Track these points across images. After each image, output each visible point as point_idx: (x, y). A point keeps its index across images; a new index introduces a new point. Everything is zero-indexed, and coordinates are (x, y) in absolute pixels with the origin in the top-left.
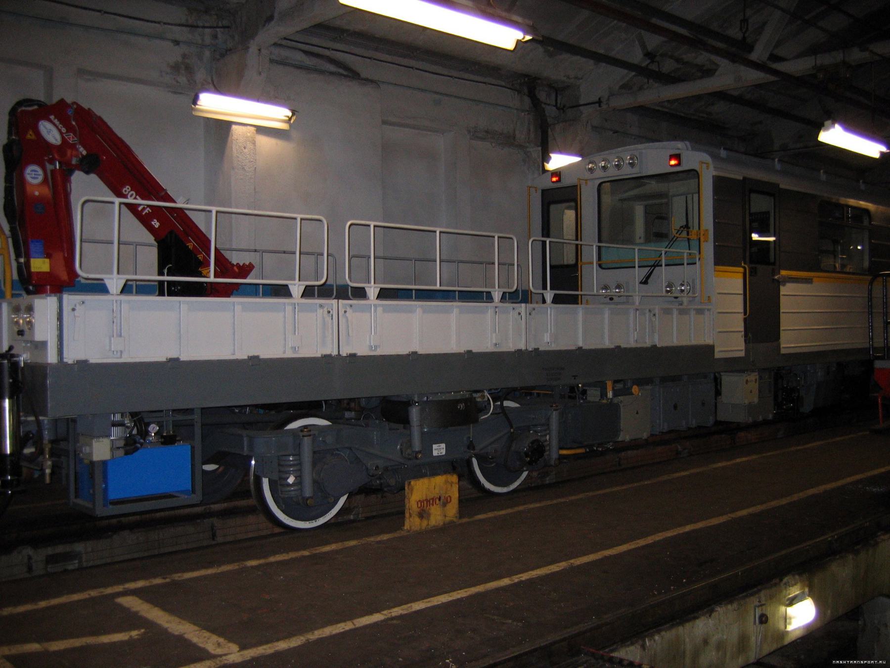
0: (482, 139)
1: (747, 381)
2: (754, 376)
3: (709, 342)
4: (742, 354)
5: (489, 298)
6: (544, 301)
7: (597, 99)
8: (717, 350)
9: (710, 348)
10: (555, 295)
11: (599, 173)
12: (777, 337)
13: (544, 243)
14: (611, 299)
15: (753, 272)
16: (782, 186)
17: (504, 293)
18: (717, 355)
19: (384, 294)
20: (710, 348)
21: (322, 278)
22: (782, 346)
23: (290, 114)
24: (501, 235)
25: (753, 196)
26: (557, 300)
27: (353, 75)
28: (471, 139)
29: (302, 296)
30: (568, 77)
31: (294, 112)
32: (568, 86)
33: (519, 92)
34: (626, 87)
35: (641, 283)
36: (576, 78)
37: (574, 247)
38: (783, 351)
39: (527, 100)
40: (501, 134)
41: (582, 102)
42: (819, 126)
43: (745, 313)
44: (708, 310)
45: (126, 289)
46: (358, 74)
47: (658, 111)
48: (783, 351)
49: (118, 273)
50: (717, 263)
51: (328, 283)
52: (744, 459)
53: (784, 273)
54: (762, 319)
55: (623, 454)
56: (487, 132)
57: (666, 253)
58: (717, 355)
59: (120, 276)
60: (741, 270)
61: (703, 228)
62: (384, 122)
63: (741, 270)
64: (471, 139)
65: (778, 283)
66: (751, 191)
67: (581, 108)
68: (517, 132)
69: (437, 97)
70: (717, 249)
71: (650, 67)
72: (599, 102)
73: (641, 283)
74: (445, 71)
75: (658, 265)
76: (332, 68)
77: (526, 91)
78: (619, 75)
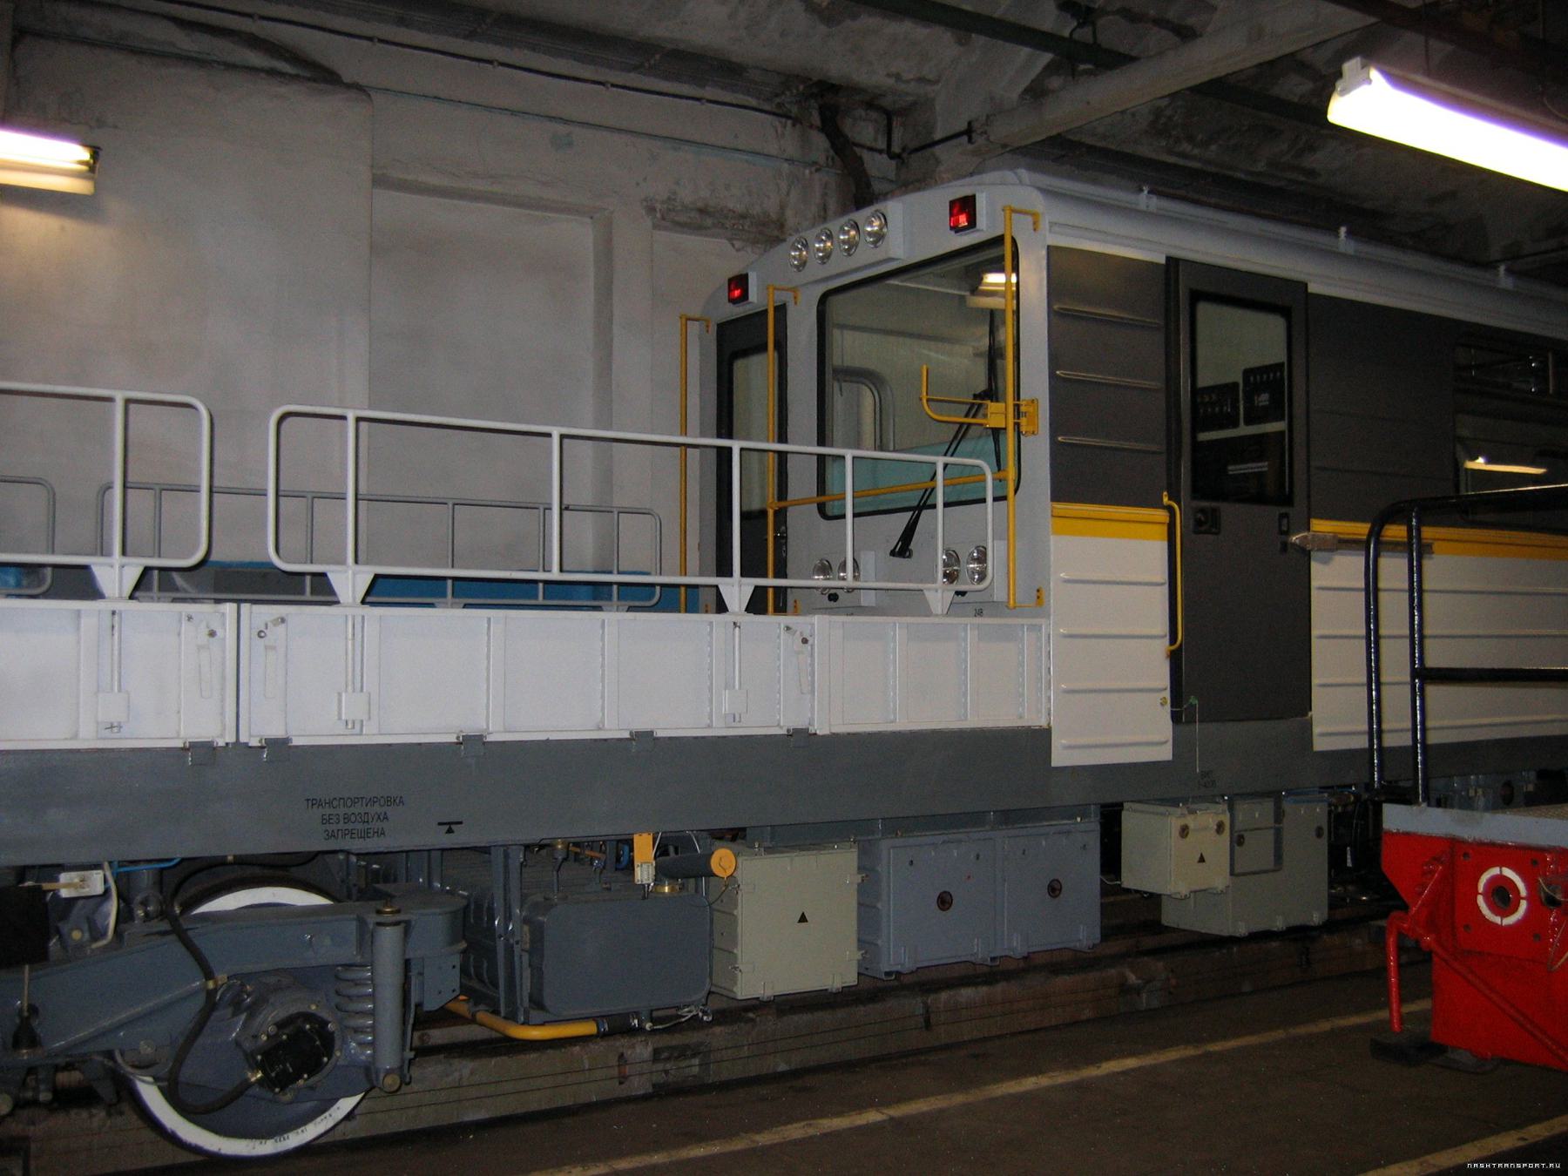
0: (697, 229)
1: (1184, 831)
2: (1206, 819)
3: (1033, 718)
4: (1165, 753)
5: (321, 590)
6: (721, 608)
7: (963, 126)
8: (1058, 743)
9: (1041, 737)
10: (757, 588)
11: (815, 270)
12: (1303, 703)
13: (724, 455)
14: (833, 597)
15: (1204, 523)
16: (1313, 288)
17: (147, 570)
18: (1059, 758)
19: (382, 591)
20: (1041, 737)
21: (196, 548)
22: (1316, 730)
23: (85, 155)
24: (565, 431)
25: (1205, 310)
26: (757, 604)
27: (323, 76)
28: (656, 227)
29: (747, 610)
30: (898, 77)
31: (95, 153)
32: (915, 103)
33: (796, 121)
34: (1036, 92)
35: (893, 553)
36: (921, 80)
37: (772, 461)
38: (1320, 745)
39: (820, 142)
40: (743, 217)
41: (938, 136)
42: (1327, 84)
43: (1173, 639)
44: (1073, 632)
45: (141, 587)
46: (339, 77)
47: (1175, 166)
48: (1320, 745)
49: (124, 553)
50: (1057, 496)
51: (214, 557)
52: (1131, 1063)
53: (1321, 526)
54: (1235, 656)
55: (944, 995)
56: (703, 211)
57: (946, 466)
58: (1059, 758)
59: (360, 568)
60: (1161, 515)
61: (1025, 395)
62: (380, 181)
63: (1161, 515)
64: (656, 227)
65: (1305, 555)
66: (1196, 297)
67: (938, 150)
68: (789, 213)
69: (562, 129)
70: (1060, 456)
71: (1076, 36)
72: (969, 132)
73: (893, 553)
74: (587, 72)
75: (926, 504)
76: (255, 58)
77: (816, 119)
78: (1026, 63)
